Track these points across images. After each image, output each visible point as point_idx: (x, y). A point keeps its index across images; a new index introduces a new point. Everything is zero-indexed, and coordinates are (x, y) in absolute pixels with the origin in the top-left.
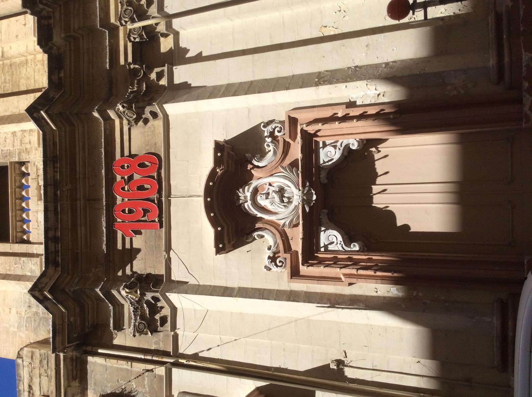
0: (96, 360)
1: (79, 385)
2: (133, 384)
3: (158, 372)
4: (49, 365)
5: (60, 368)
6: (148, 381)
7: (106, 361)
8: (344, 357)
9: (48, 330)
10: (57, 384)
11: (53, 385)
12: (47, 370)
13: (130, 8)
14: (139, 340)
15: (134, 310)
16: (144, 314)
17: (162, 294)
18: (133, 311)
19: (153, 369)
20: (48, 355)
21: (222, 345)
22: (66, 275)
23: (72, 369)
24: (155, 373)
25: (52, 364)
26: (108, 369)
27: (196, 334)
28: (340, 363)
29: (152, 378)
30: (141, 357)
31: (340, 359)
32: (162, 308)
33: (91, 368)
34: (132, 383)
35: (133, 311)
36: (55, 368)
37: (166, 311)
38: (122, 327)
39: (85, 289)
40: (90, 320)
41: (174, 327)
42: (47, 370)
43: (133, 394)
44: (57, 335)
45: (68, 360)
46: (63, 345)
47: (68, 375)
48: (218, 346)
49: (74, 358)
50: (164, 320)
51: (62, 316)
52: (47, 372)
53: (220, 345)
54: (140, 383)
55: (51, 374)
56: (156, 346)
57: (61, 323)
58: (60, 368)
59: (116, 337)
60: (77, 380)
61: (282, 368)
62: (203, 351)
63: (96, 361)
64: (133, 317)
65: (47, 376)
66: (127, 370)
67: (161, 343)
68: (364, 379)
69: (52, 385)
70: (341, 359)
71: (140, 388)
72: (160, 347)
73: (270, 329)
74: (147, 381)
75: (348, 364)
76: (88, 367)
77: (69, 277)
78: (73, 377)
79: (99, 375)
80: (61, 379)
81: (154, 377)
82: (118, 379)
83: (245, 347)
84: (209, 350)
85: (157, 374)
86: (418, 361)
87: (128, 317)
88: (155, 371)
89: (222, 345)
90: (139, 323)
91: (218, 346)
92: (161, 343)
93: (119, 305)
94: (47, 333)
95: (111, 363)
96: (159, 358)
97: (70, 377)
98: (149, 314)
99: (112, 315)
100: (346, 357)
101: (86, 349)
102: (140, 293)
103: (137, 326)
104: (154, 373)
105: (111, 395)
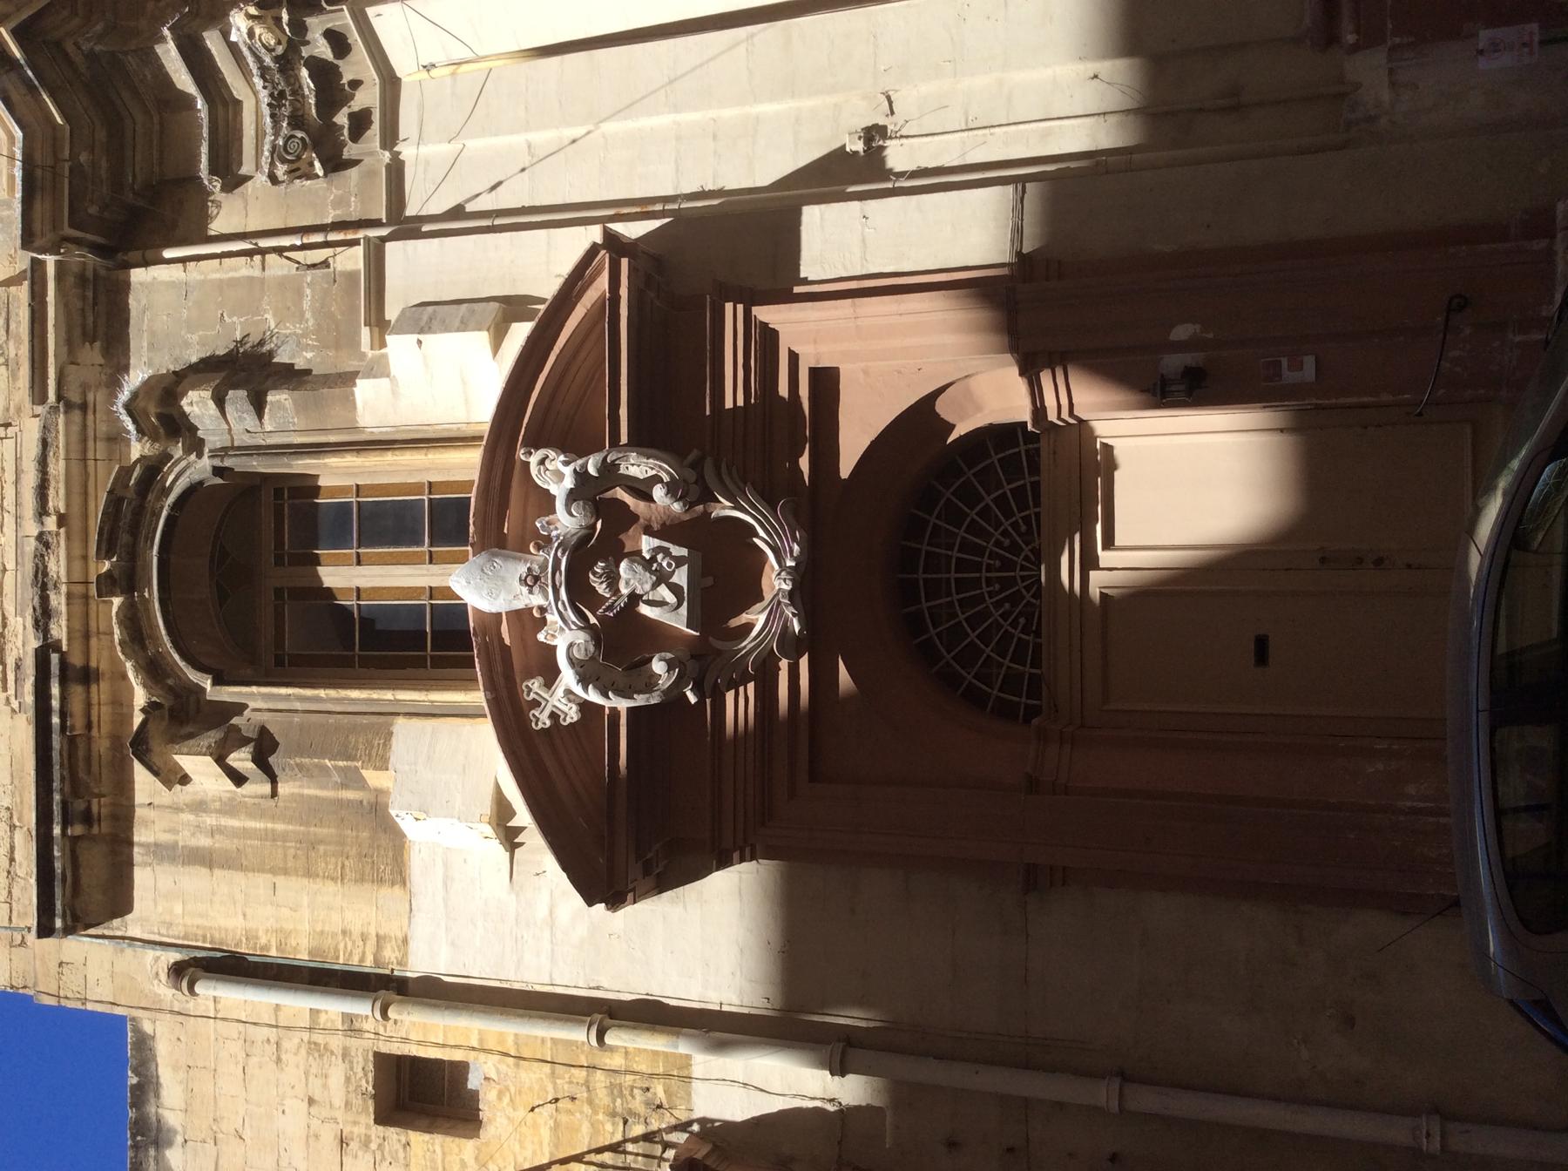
0: (156, 275)
1: (102, 361)
2: (268, 317)
3: (344, 263)
4: (11, 328)
5: (44, 304)
6: (313, 297)
7: (185, 271)
8: (887, 116)
9: (11, 256)
10: (36, 349)
11: (21, 386)
12: (4, 345)
13: (300, 134)
14: (288, 206)
15: (273, 102)
16: (302, 116)
17: (356, 11)
18: (268, 105)
19: (327, 259)
20: (8, 300)
21: (535, 164)
22: (65, 13)
23: (83, 310)
24: (335, 269)
25: (20, 322)
26: (192, 292)
27: (455, 146)
28: (874, 134)
29: (326, 286)
30: (292, 243)
31: (874, 123)
32: (355, 84)
33: (139, 301)
34: (266, 316)
35: (268, 105)
36: (30, 304)
37: (368, 97)
38: (234, 168)
39: (126, 53)
40: (137, 169)
41: (390, 137)
42: (4, 345)
43: (266, 348)
44: (38, 197)
45: (72, 279)
46: (54, 227)
47: (69, 331)
48: (523, 170)
49: (89, 274)
50: (360, 122)
51: (55, 139)
52: (6, 352)
53: (527, 165)
54: (289, 308)
55: (16, 355)
56: (338, 212)
57: (50, 162)
58: (46, 302)
59: (218, 213)
60: (97, 344)
61: (710, 191)
62: (477, 195)
63: (154, 278)
64: (267, 131)
65: (6, 364)
66: (251, 279)
67: (353, 199)
68: (940, 165)
69: (19, 388)
70: (877, 124)
71: (288, 325)
72: (351, 212)
73: (676, 79)
74: (309, 298)
75: (897, 132)
76: (130, 301)
77: (76, 21)
78: (84, 334)
79: (165, 317)
80: (47, 338)
81: (332, 280)
82: (222, 315)
83: (602, 155)
84: (494, 188)
85: (340, 272)
86: (1092, 75)
87: (254, 135)
88: (334, 262)
89: (535, 164)
90: (289, 138)
91: (523, 170)
92: (353, 199)
93: (225, 104)
94: (7, 264)
95: (202, 273)
96: (345, 234)
97: (77, 332)
98: (317, 105)
99: (205, 134)
100: (892, 113)
101: (126, 258)
102: (289, 19)
103: (279, 149)
104: (332, 269)
105: (201, 365)
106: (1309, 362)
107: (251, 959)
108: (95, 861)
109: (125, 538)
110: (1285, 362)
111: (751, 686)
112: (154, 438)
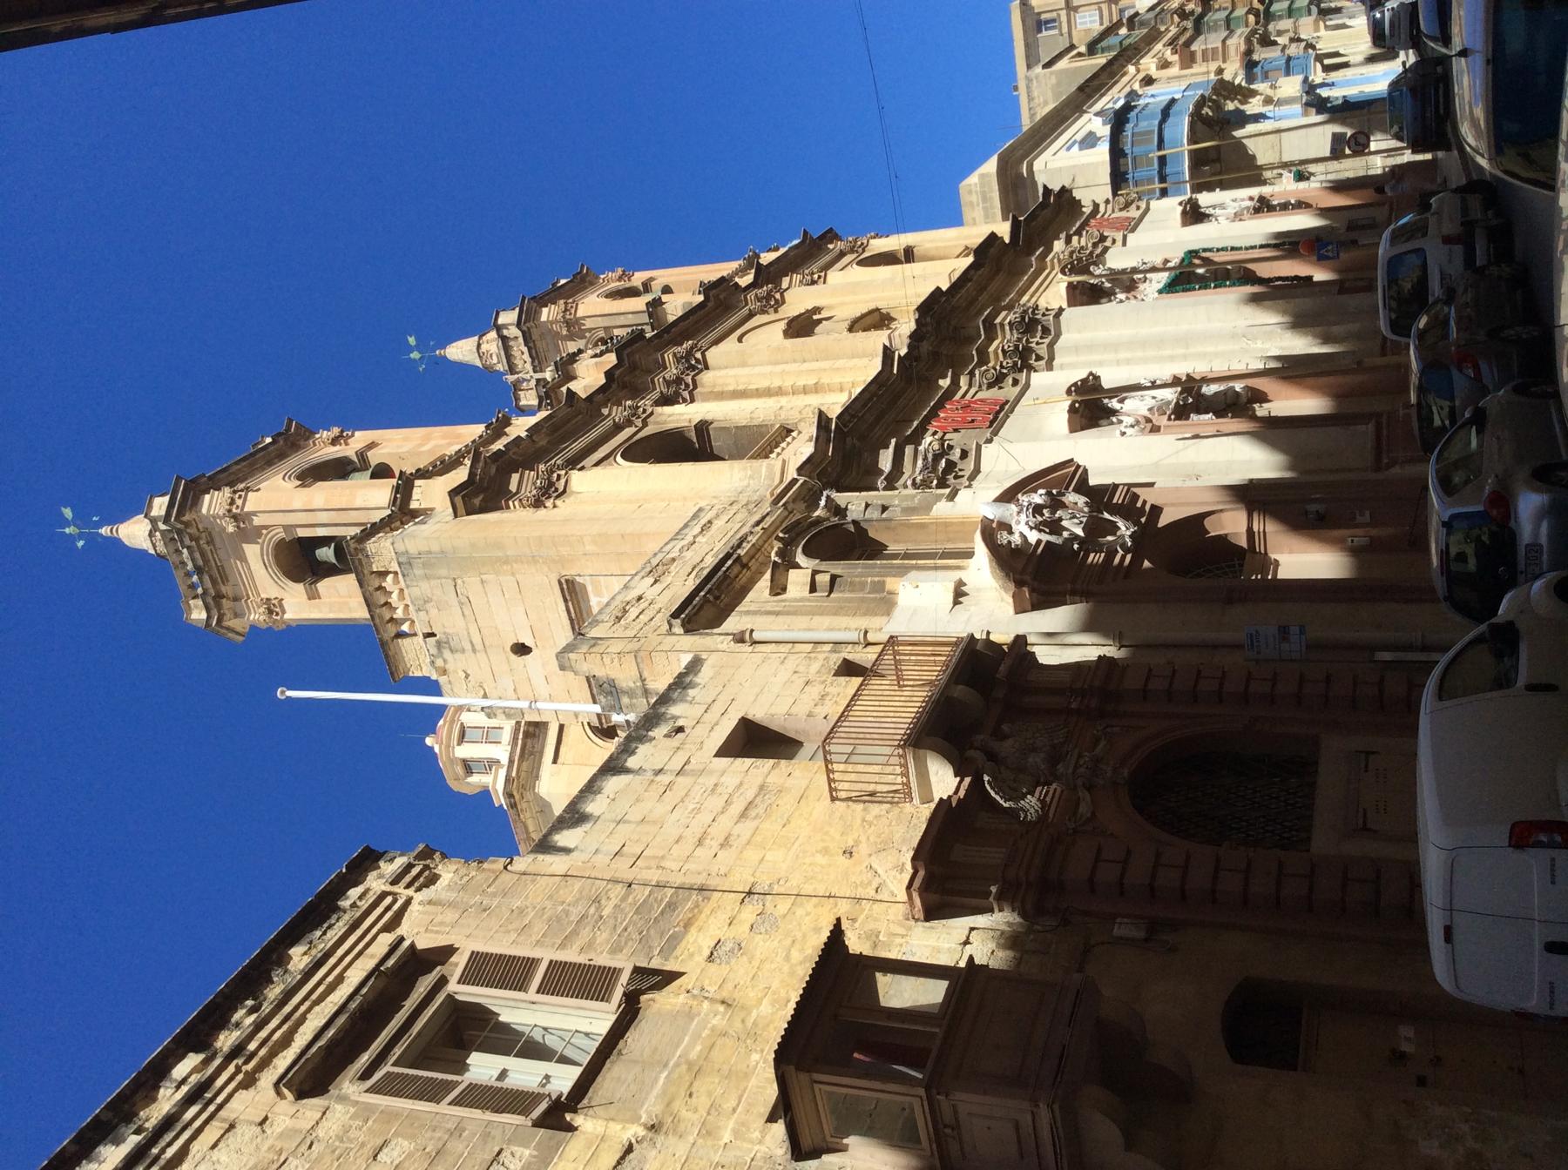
106: (1367, 513)
107: (513, 1026)
108: (709, 612)
109: (793, 535)
110: (1357, 512)
111: (1103, 555)
112: (829, 511)
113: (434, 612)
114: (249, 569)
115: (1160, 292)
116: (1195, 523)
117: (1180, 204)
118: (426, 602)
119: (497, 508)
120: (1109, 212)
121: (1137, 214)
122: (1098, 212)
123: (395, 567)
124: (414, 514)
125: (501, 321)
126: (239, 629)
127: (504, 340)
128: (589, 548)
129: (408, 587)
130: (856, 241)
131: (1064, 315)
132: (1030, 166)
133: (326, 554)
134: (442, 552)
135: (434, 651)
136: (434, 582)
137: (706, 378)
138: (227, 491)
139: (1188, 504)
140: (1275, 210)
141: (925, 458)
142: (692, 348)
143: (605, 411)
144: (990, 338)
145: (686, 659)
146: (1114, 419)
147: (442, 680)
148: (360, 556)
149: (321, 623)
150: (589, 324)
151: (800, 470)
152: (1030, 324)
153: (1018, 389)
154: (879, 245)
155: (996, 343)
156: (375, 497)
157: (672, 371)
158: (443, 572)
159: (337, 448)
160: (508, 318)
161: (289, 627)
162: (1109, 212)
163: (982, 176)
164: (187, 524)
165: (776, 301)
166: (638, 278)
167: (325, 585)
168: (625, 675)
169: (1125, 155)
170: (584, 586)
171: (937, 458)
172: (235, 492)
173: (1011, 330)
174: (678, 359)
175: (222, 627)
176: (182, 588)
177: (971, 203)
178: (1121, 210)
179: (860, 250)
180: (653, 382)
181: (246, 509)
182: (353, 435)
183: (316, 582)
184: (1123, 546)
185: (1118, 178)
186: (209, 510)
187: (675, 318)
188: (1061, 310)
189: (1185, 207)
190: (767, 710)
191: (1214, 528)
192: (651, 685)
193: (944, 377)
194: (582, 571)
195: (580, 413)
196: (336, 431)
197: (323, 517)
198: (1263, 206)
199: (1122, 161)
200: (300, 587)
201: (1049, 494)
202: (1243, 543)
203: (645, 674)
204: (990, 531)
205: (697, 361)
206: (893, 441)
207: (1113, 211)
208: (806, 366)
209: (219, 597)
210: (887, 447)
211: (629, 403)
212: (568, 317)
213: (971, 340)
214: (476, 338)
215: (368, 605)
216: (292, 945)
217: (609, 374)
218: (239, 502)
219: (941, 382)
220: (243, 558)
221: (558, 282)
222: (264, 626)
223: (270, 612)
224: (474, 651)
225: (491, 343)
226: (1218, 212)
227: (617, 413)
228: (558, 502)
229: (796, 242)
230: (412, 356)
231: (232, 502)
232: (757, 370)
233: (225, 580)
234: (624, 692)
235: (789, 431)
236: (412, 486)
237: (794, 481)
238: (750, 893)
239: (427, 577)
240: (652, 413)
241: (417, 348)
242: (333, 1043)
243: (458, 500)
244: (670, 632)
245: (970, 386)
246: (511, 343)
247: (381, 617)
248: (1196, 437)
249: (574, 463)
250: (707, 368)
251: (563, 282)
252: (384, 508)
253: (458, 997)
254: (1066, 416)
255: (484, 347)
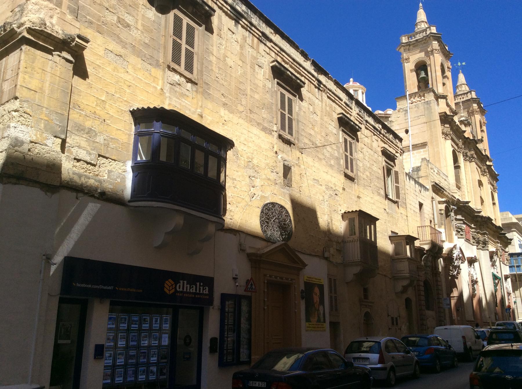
113: (415, 109)
114: (418, 53)
115: (493, 273)
116: (455, 286)
117: (475, 256)
118: (418, 108)
119: (441, 123)
120: (506, 256)
121: (505, 263)
122: (506, 253)
123: (426, 100)
124: (437, 100)
125: (472, 92)
126: (400, 50)
127: (425, 30)
128: (436, 150)
129: (421, 103)
130: (496, 189)
131: (487, 251)
132: (515, 231)
133: (423, 75)
134: (432, 112)
135: (404, 109)
136: (423, 110)
137: (468, 163)
138: (439, 48)
139: (459, 285)
140: (472, 287)
141: (460, 226)
142: (475, 158)
143: (460, 140)
144: (481, 234)
145: (428, 187)
146: (470, 267)
147: (397, 111)
148: (429, 91)
149: (404, 71)
150: (473, 118)
151: (458, 199)
152: (485, 243)
153: (472, 243)
154: (496, 195)
155: (480, 235)
156: (440, 90)
157: (469, 154)
158: (426, 112)
159: (447, 69)
160: (434, 30)
161: (402, 64)
162: (506, 256)
163: (511, 218)
164: (429, 38)
165: (484, 174)
166: (484, 128)
167: (414, 74)
168: (421, 173)
169: (518, 257)
170: (425, 148)
171: (461, 229)
172: (439, 50)
173: (484, 239)
174: (472, 155)
175: (401, 47)
176: (411, 34)
177: (503, 215)
178: (506, 259)
179: (494, 190)
180: (466, 149)
181: (435, 54)
182: (450, 72)
183: (415, 71)
184: (453, 273)
185: (512, 255)
186: (434, 44)
187: (478, 146)
188: (488, 250)
189: (474, 258)
190: (424, 207)
191: (454, 290)
192: (420, 179)
193: (474, 225)
194: (429, 147)
195: (460, 134)
196: (451, 67)
197: (434, 75)
198: (509, 294)
199: (516, 256)
200: (413, 68)
201: (461, 257)
202: (451, 296)
203: (423, 178)
204: (455, 247)
205: (472, 160)
206: (464, 218)
207: (472, 234)
208: (472, 188)
209: (409, 45)
210: (462, 217)
211: (463, 147)
212: (434, 51)
213: (480, 229)
214: (466, 83)
215: (416, 93)
216: (393, 135)
217: (468, 138)
218: (436, 52)
219: (473, 225)
220: (420, 52)
221: (482, 104)
222: (402, 57)
223: (406, 59)
224: (405, 120)
225: (424, 26)
226: (507, 283)
227: (460, 143)
228: (444, 138)
229: (496, 173)
230: (459, 63)
231: (436, 50)
232: (470, 176)
233: (414, 47)
234: (418, 173)
235: (459, 189)
236: (444, 99)
237: (455, 198)
238: (407, 216)
239: (424, 108)
240: (461, 153)
241: (462, 65)
242: (387, 152)
243: (444, 114)
244: (431, 182)
245: (472, 232)
246: (466, 95)
247: (412, 96)
248: (469, 285)
249: (452, 140)
250: (470, 162)
251: (447, 48)
252: (438, 92)
253: (392, 171)
254: (471, 256)
255: (463, 86)
